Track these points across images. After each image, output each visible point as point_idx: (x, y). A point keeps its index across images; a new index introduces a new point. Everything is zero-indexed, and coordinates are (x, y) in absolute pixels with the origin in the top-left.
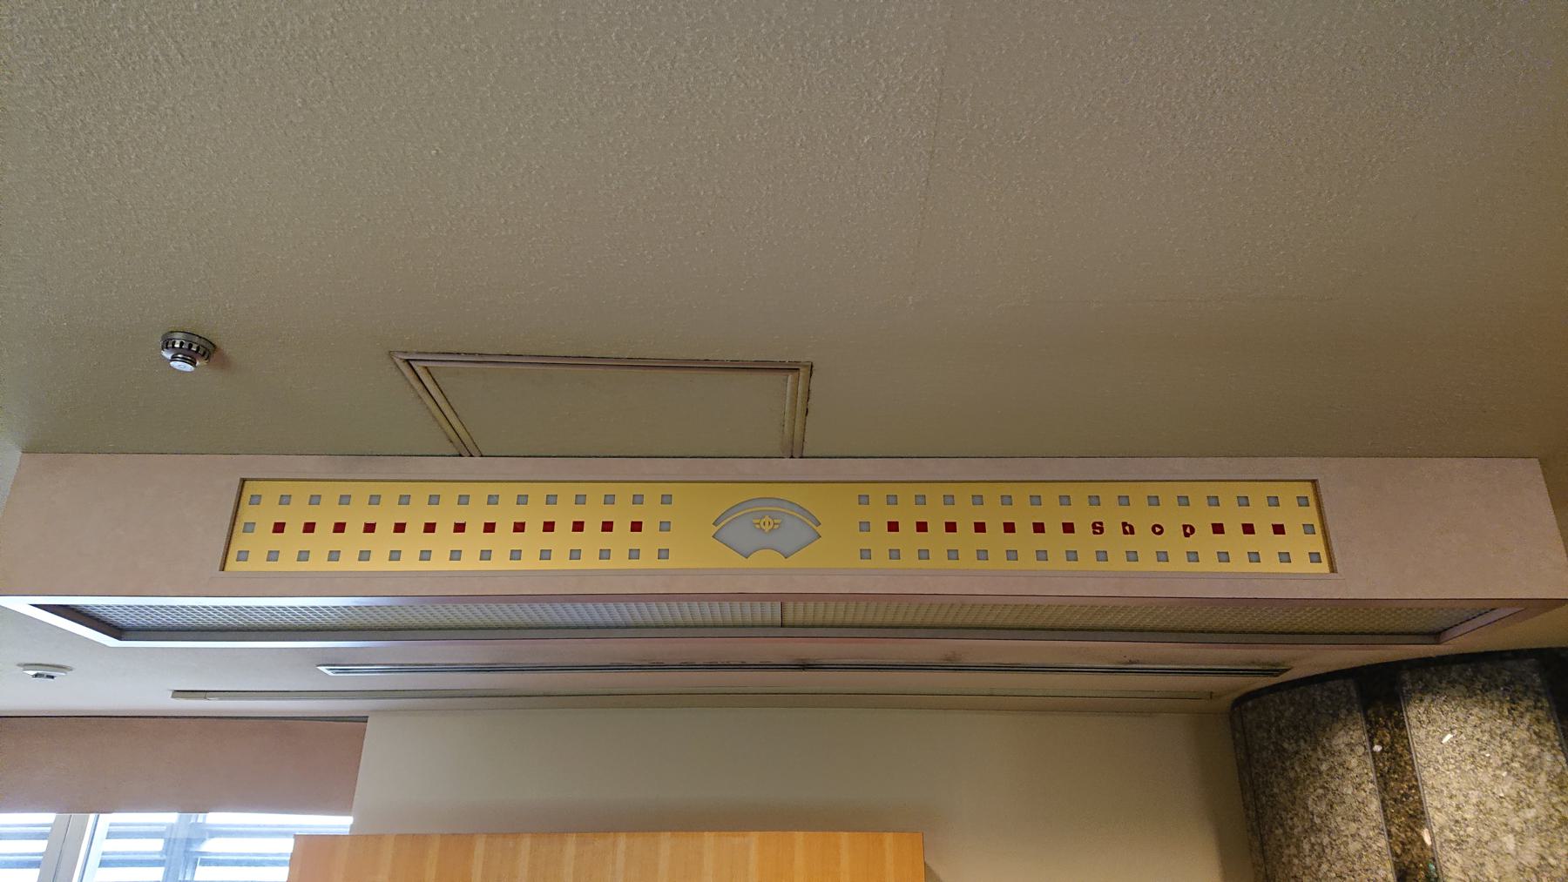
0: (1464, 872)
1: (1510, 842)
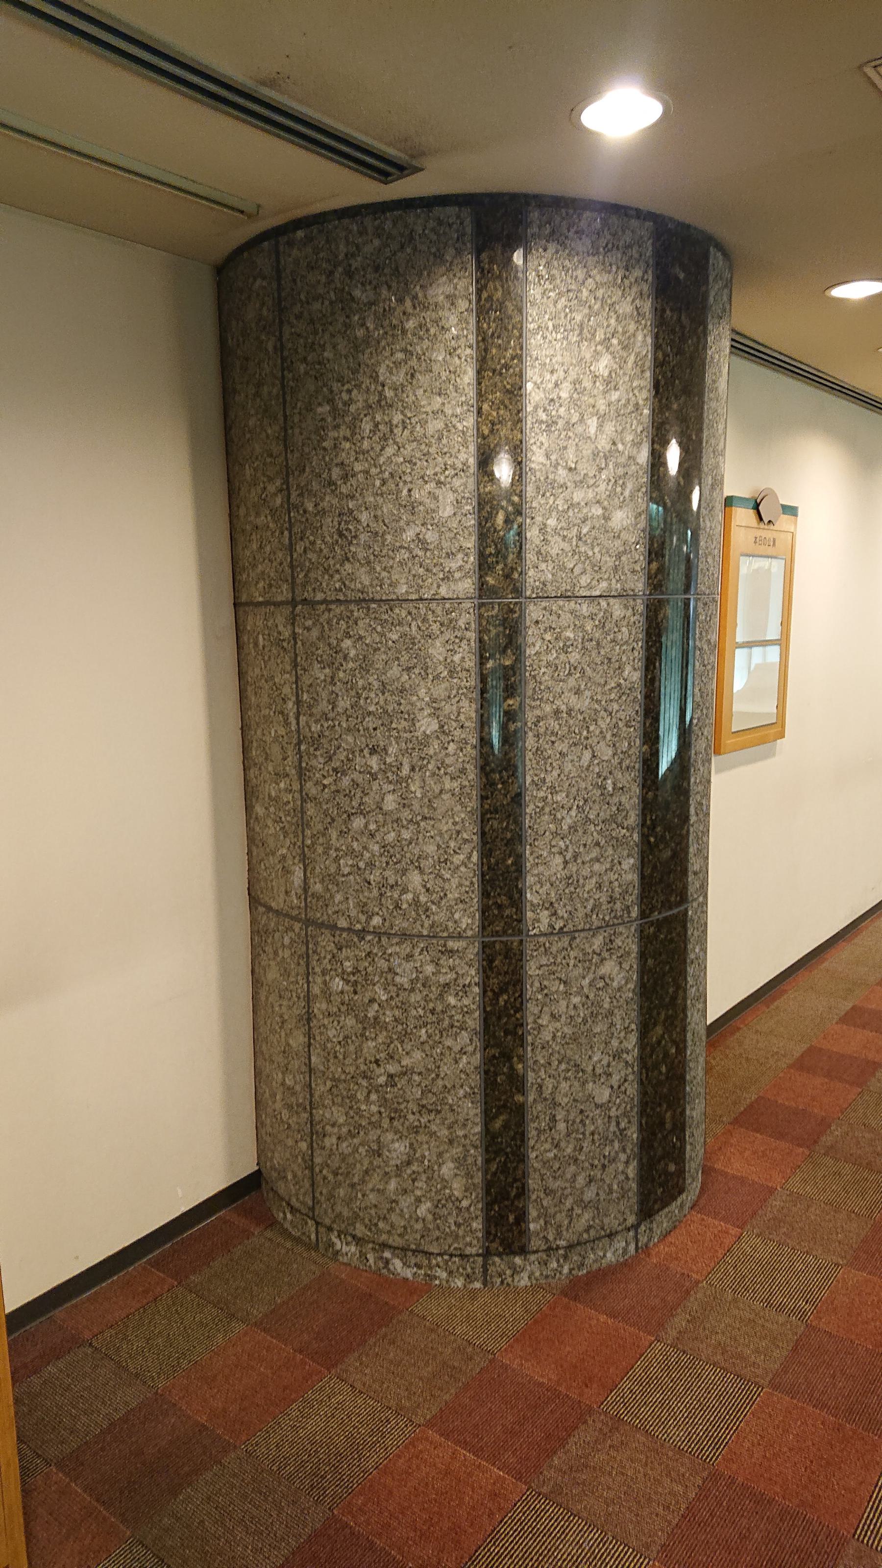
0: (547, 456)
1: (592, 424)
